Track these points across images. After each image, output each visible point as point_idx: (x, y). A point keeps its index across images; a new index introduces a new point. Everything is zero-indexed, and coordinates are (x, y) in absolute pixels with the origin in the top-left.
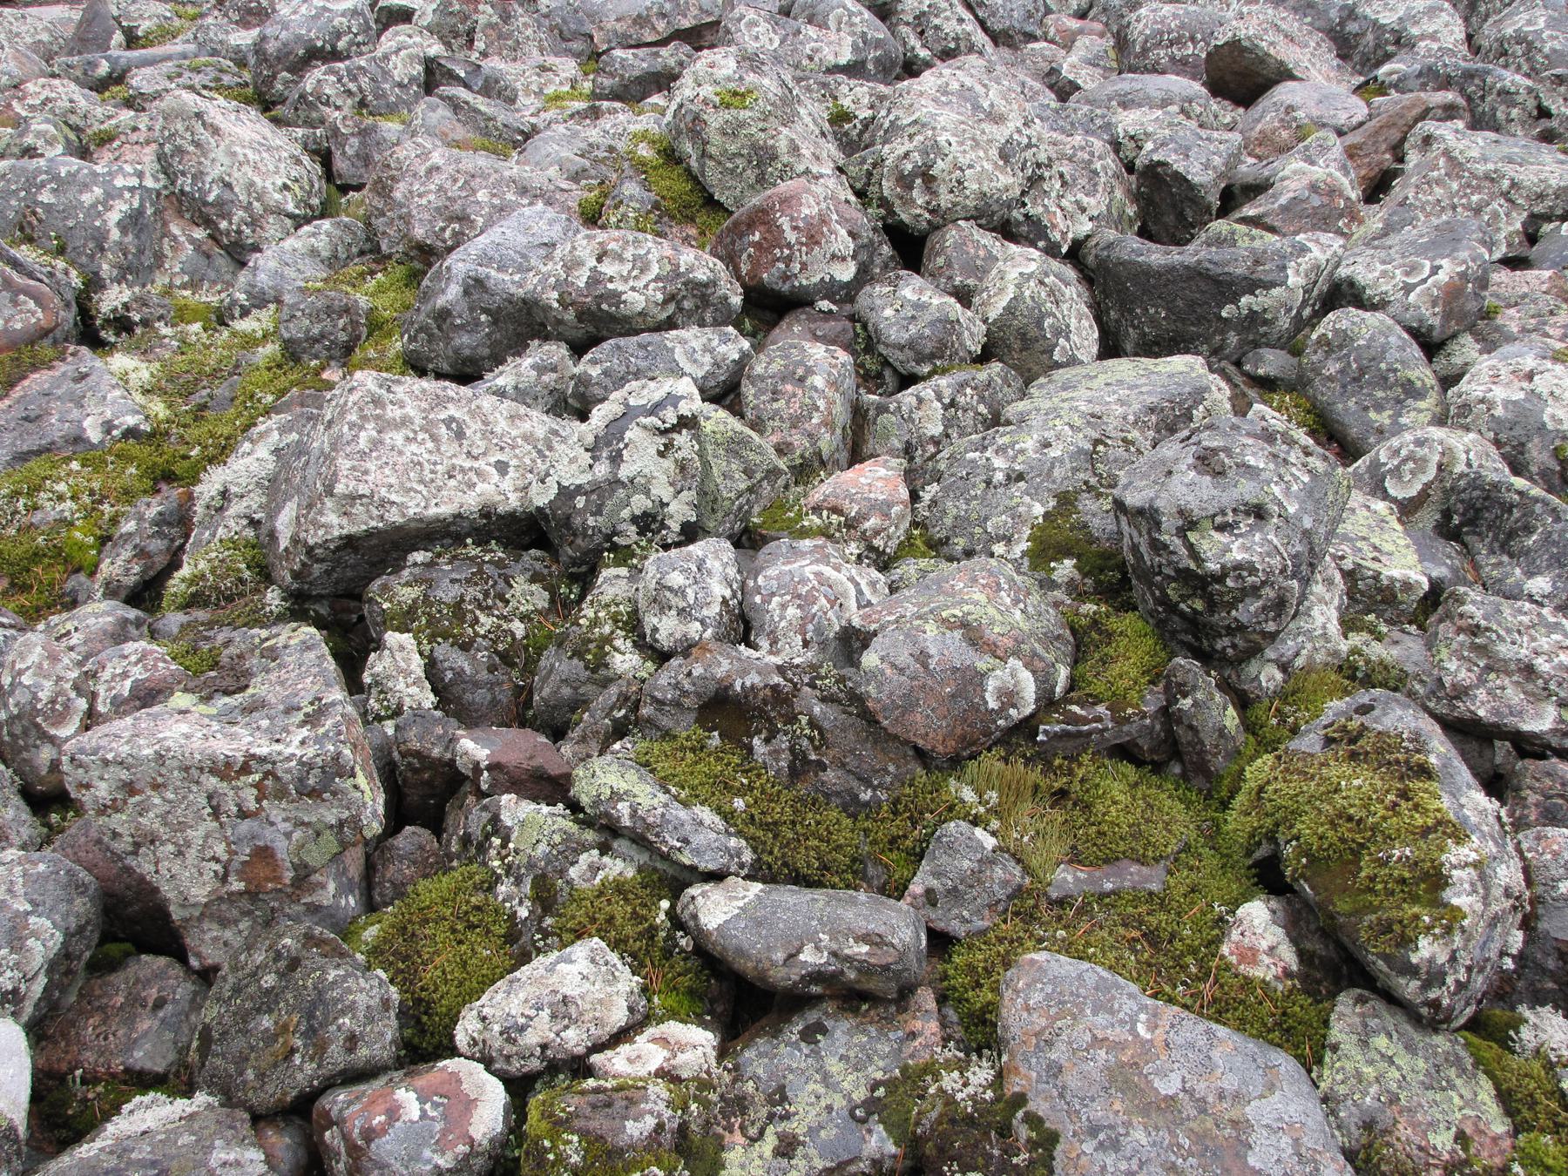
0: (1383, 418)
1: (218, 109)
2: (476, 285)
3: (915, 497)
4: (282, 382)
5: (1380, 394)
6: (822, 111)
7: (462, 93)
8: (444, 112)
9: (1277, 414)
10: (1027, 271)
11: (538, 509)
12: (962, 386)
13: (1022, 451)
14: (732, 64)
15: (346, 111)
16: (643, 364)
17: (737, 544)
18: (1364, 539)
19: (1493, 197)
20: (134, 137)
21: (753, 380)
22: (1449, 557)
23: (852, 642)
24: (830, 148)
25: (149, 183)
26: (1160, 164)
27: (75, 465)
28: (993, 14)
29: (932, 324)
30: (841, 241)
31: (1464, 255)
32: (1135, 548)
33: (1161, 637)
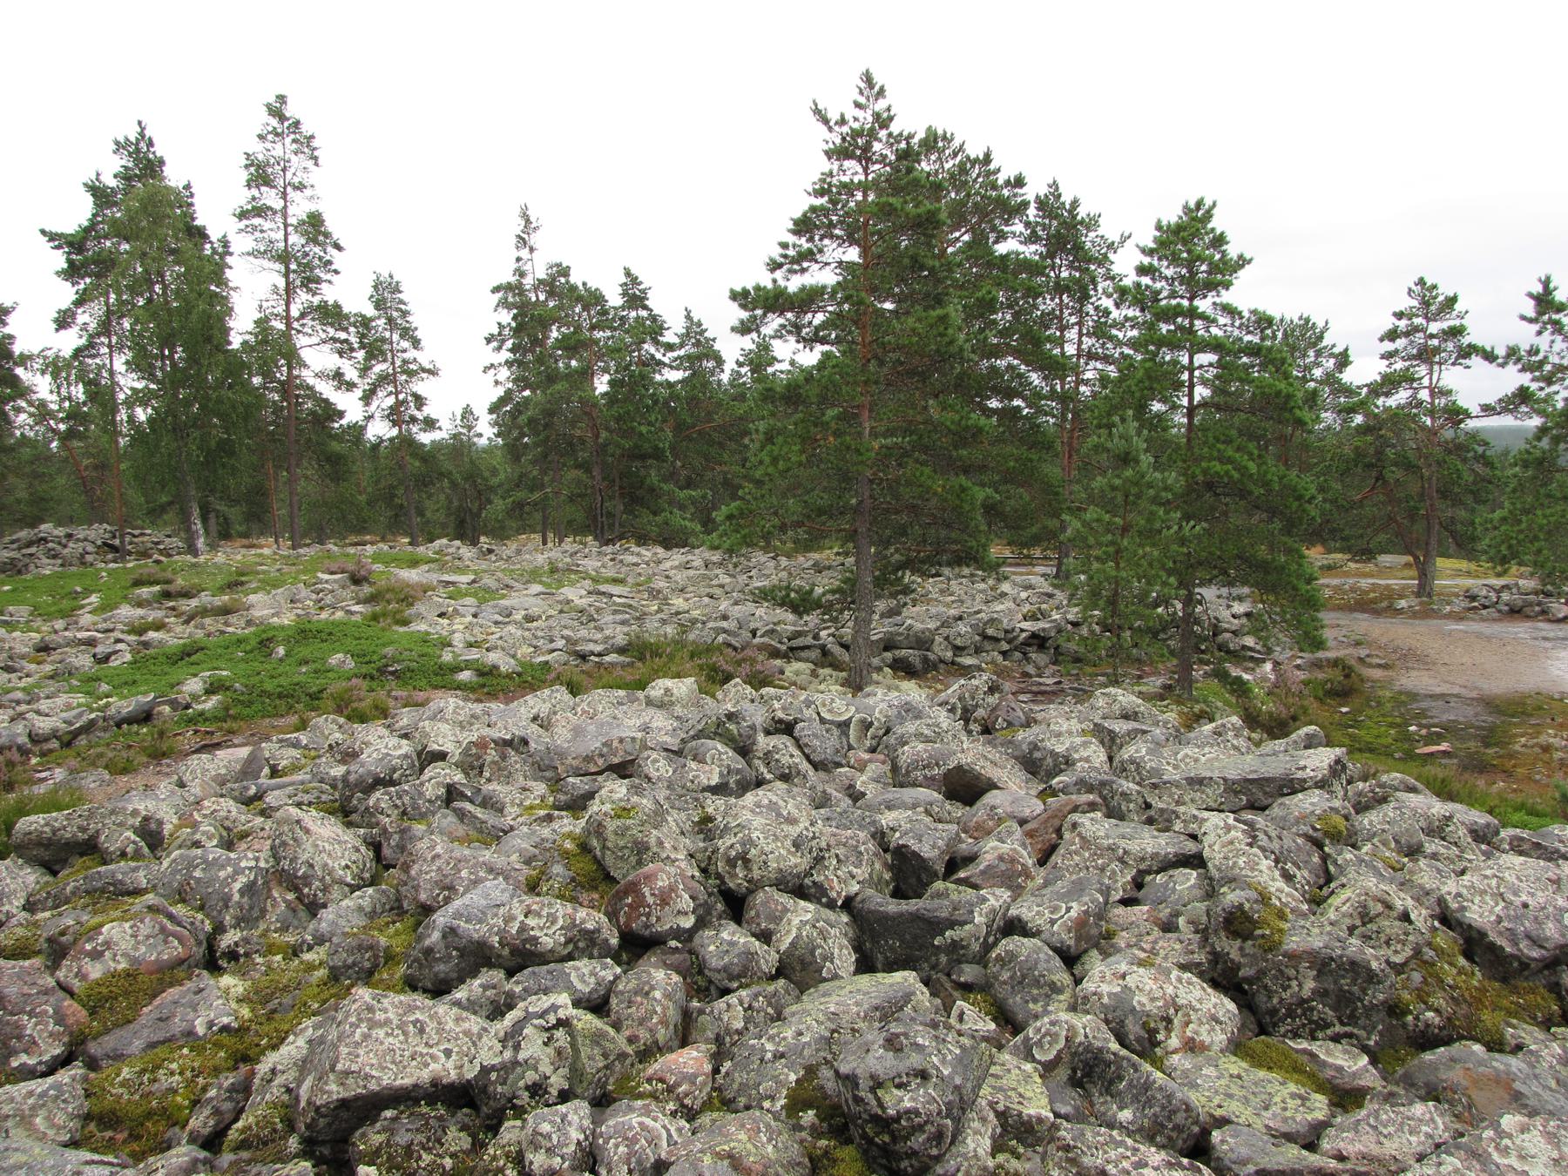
0: (1037, 1007)
1: (311, 818)
2: (450, 932)
3: (716, 1071)
4: (326, 995)
5: (1035, 992)
7: (468, 806)
11: (468, 1081)
12: (756, 996)
13: (784, 1039)
14: (624, 790)
15: (393, 817)
16: (549, 984)
19: (1111, 861)
20: (261, 834)
25: (262, 864)
27: (185, 1051)
29: (739, 955)
30: (686, 902)
31: (1086, 899)
33: (867, 1161)
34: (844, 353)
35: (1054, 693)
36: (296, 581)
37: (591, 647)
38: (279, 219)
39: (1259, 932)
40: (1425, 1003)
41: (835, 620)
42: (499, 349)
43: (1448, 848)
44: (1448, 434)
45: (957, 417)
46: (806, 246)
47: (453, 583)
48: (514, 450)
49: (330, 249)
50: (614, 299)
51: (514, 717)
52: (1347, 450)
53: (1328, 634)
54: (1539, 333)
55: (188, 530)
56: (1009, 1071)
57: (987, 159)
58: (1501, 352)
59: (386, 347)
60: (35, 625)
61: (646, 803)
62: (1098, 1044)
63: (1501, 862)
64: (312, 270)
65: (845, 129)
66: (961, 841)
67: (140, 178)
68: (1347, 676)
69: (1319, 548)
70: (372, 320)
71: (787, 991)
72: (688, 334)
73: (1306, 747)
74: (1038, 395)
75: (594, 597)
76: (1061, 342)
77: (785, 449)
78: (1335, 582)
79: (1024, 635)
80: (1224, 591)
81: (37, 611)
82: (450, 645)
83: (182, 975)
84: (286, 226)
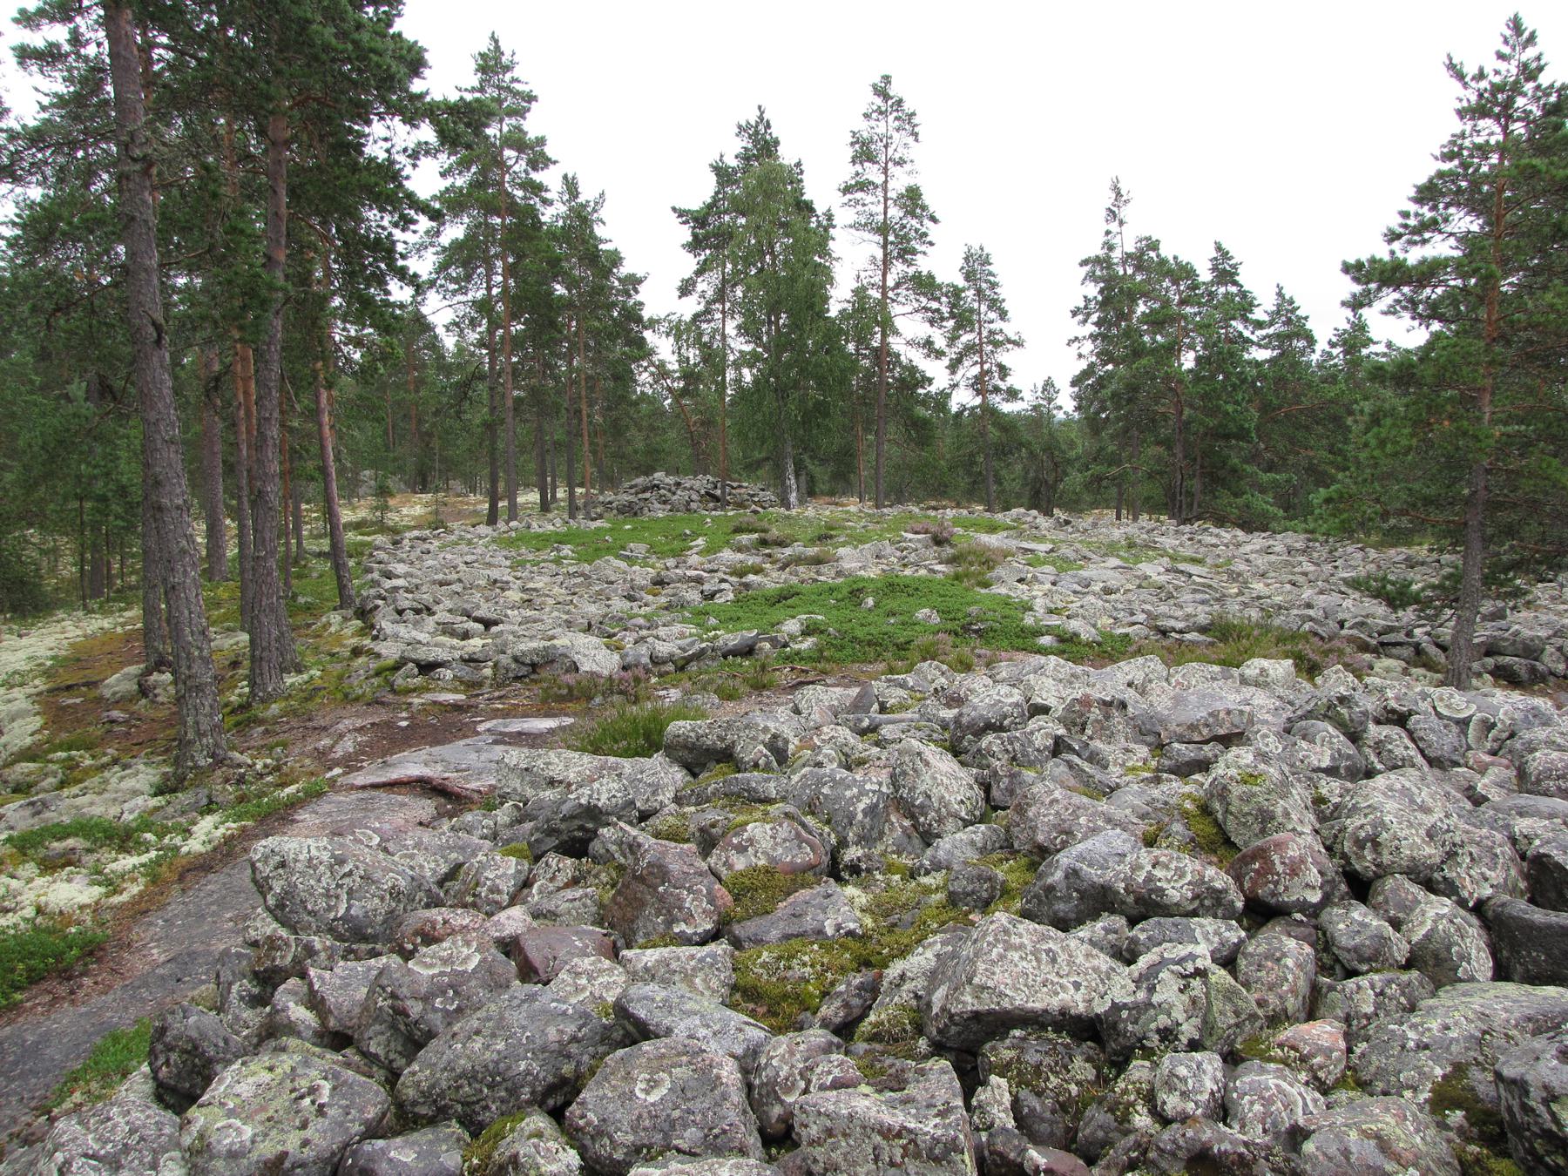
1: (931, 752)
2: (1072, 874)
3: (1349, 1050)
4: (944, 917)
6: (1308, 796)
8: (1063, 768)
11: (1097, 1015)
12: (1389, 982)
13: (1429, 1030)
14: (1251, 757)
16: (1174, 936)
17: (1225, 1060)
21: (1245, 955)
23: (1297, 1136)
24: (1311, 817)
25: (884, 789)
26: (1545, 855)
27: (816, 947)
29: (1371, 937)
30: (1313, 876)
32: (1509, 1109)
36: (881, 538)
37: (1172, 623)
38: (880, 193)
42: (1085, 321)
47: (1032, 551)
48: (1093, 425)
49: (926, 221)
50: (1205, 275)
51: (1114, 680)
55: (783, 483)
59: (975, 317)
60: (651, 561)
64: (909, 241)
65: (1484, 84)
67: (757, 158)
70: (963, 290)
72: (1278, 312)
77: (1394, 432)
81: (652, 549)
82: (1031, 609)
83: (812, 879)
84: (886, 199)
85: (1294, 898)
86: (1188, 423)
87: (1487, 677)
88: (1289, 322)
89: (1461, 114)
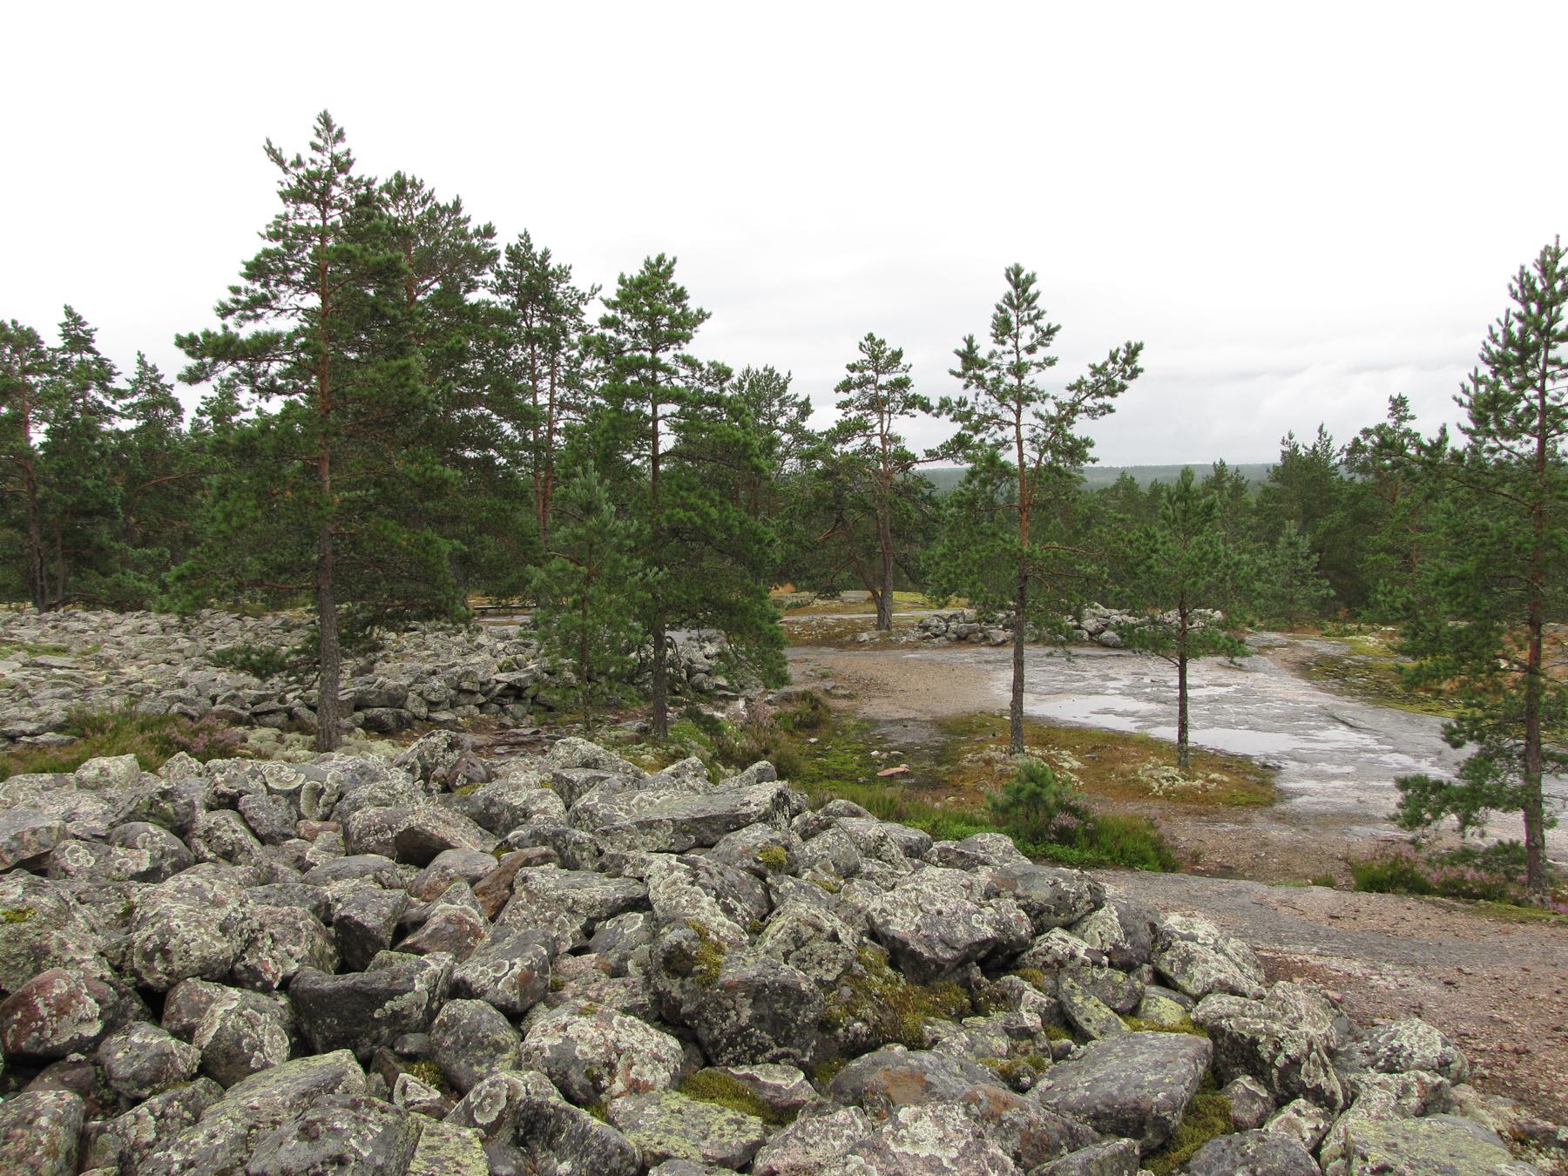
5: (479, 1054)
9: (415, 1078)
10: (230, 1008)
12: (170, 1101)
13: (195, 1145)
14: (19, 890)
18: (451, 1158)
22: (516, 1159)
26: (347, 917)
28: (260, 824)
29: (151, 1058)
30: (91, 1007)
31: (530, 953)
34: (308, 401)
35: (531, 743)
37: (23, 726)
39: (697, 968)
40: (854, 1015)
41: (300, 681)
43: (883, 867)
44: (898, 477)
45: (421, 469)
46: (260, 291)
50: (52, 339)
52: (808, 494)
53: (792, 670)
54: (966, 387)
56: (448, 1140)
57: (457, 207)
58: (935, 403)
61: (47, 902)
62: (538, 1099)
63: (923, 875)
65: (301, 171)
66: (411, 905)
68: (815, 708)
69: (789, 587)
71: (208, 1091)
72: (141, 381)
73: (758, 782)
74: (510, 444)
75: (31, 670)
76: (534, 391)
77: (239, 505)
78: (804, 619)
79: (500, 686)
80: (694, 633)
85: (67, 1038)
86: (45, 501)
87: (359, 730)
88: (153, 390)
89: (284, 196)
